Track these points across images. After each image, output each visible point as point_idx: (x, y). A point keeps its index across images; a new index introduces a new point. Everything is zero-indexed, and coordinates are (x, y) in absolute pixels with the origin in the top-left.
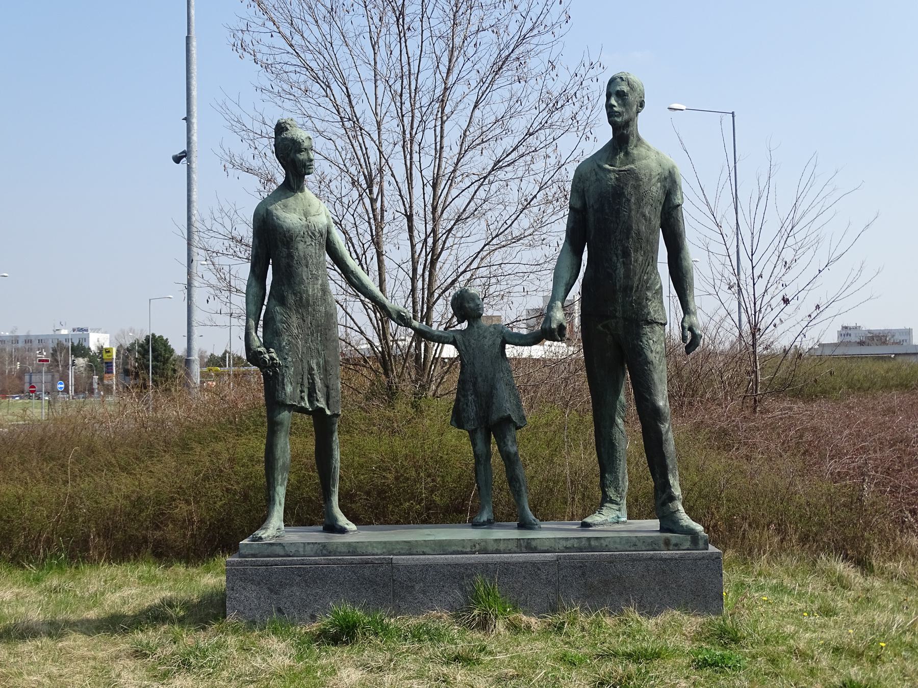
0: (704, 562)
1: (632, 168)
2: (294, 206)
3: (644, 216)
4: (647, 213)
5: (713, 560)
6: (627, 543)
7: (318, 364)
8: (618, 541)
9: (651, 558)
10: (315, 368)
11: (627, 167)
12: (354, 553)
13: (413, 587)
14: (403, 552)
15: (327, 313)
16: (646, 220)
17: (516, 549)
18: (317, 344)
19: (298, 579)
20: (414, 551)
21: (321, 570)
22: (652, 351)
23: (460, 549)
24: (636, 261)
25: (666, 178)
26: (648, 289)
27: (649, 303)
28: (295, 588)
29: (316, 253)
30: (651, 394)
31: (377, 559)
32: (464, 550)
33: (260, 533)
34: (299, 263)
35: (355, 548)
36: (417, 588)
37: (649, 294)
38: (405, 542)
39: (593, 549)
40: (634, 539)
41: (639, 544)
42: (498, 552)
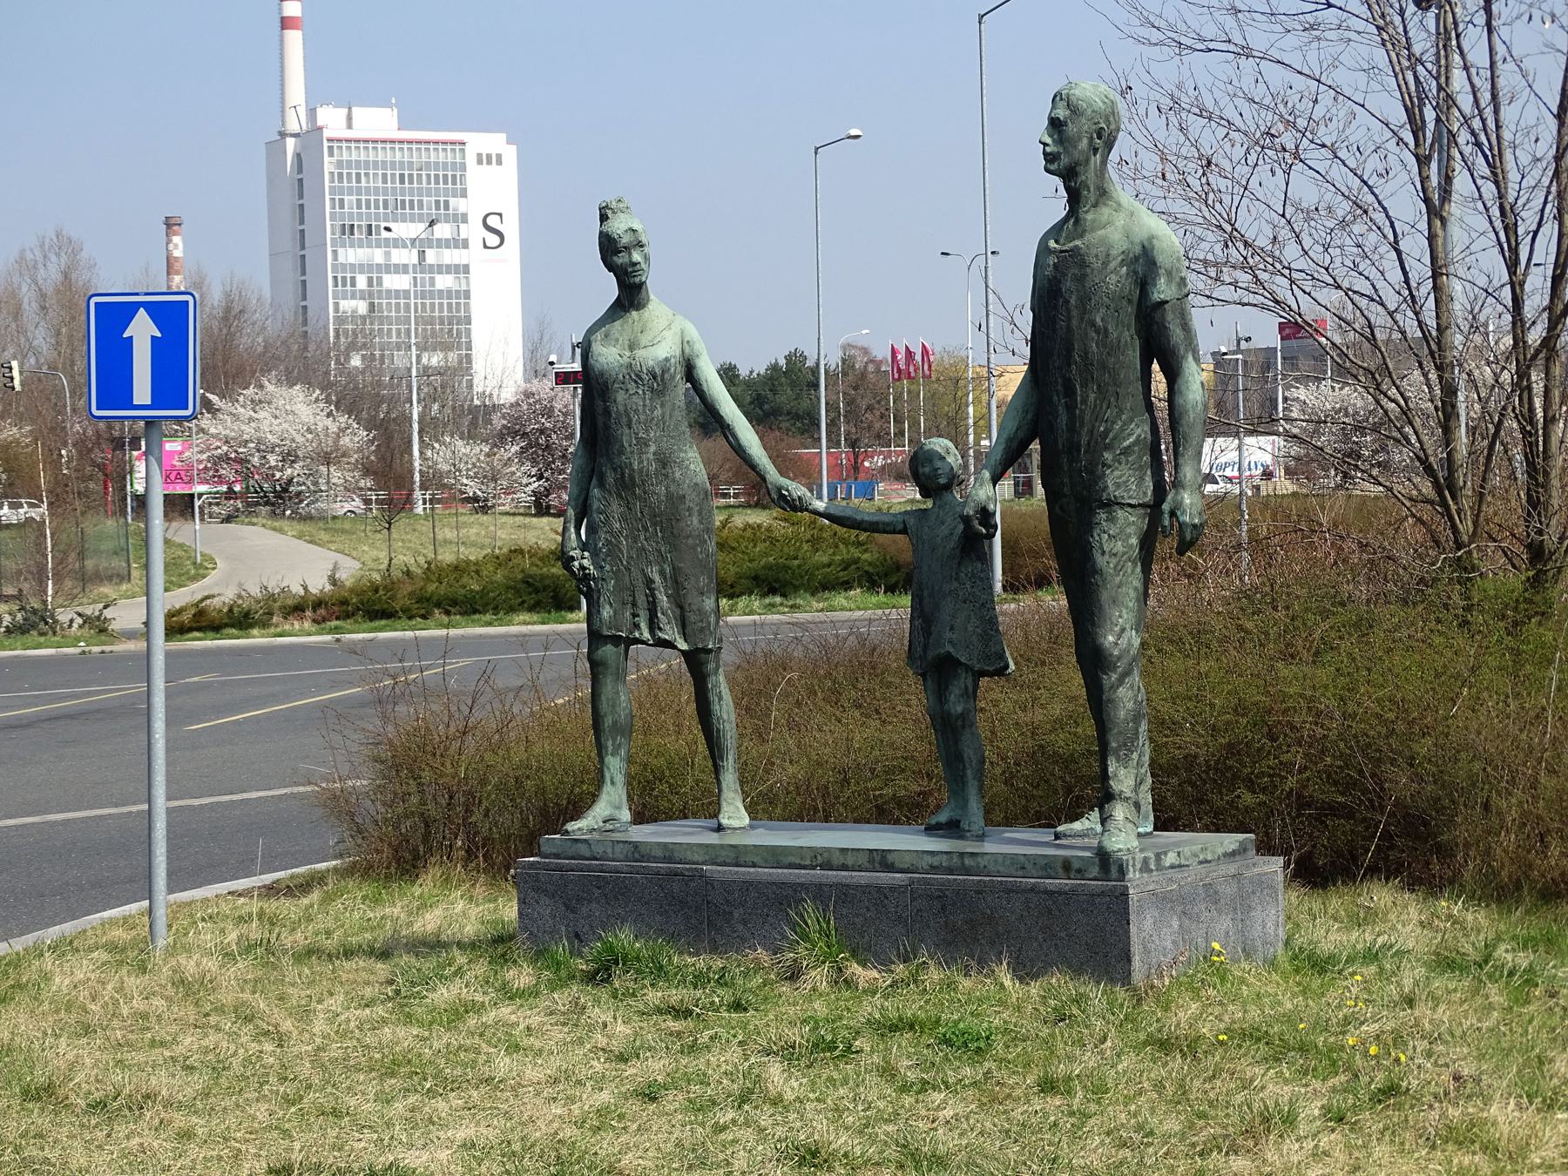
0: (1104, 900)
1: (1076, 246)
2: (617, 335)
3: (1093, 324)
4: (1098, 320)
5: (1117, 898)
6: (1012, 864)
7: (662, 573)
8: (1000, 859)
9: (1032, 890)
10: (657, 578)
11: (1071, 245)
12: (669, 860)
13: (731, 913)
14: (728, 861)
15: (669, 496)
16: (1098, 332)
17: (867, 865)
18: (657, 543)
19: (597, 892)
20: (742, 861)
21: (623, 882)
22: (1103, 553)
23: (798, 861)
24: (1084, 401)
25: (1136, 258)
26: (1108, 447)
27: (1108, 472)
28: (594, 905)
29: (644, 405)
30: (1093, 624)
31: (687, 870)
32: (803, 863)
33: (571, 826)
34: (618, 423)
35: (672, 851)
36: (736, 915)
37: (1108, 456)
38: (731, 846)
39: (967, 871)
40: (1022, 858)
41: (1029, 866)
42: (844, 868)
